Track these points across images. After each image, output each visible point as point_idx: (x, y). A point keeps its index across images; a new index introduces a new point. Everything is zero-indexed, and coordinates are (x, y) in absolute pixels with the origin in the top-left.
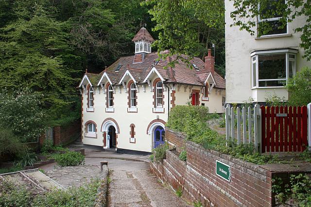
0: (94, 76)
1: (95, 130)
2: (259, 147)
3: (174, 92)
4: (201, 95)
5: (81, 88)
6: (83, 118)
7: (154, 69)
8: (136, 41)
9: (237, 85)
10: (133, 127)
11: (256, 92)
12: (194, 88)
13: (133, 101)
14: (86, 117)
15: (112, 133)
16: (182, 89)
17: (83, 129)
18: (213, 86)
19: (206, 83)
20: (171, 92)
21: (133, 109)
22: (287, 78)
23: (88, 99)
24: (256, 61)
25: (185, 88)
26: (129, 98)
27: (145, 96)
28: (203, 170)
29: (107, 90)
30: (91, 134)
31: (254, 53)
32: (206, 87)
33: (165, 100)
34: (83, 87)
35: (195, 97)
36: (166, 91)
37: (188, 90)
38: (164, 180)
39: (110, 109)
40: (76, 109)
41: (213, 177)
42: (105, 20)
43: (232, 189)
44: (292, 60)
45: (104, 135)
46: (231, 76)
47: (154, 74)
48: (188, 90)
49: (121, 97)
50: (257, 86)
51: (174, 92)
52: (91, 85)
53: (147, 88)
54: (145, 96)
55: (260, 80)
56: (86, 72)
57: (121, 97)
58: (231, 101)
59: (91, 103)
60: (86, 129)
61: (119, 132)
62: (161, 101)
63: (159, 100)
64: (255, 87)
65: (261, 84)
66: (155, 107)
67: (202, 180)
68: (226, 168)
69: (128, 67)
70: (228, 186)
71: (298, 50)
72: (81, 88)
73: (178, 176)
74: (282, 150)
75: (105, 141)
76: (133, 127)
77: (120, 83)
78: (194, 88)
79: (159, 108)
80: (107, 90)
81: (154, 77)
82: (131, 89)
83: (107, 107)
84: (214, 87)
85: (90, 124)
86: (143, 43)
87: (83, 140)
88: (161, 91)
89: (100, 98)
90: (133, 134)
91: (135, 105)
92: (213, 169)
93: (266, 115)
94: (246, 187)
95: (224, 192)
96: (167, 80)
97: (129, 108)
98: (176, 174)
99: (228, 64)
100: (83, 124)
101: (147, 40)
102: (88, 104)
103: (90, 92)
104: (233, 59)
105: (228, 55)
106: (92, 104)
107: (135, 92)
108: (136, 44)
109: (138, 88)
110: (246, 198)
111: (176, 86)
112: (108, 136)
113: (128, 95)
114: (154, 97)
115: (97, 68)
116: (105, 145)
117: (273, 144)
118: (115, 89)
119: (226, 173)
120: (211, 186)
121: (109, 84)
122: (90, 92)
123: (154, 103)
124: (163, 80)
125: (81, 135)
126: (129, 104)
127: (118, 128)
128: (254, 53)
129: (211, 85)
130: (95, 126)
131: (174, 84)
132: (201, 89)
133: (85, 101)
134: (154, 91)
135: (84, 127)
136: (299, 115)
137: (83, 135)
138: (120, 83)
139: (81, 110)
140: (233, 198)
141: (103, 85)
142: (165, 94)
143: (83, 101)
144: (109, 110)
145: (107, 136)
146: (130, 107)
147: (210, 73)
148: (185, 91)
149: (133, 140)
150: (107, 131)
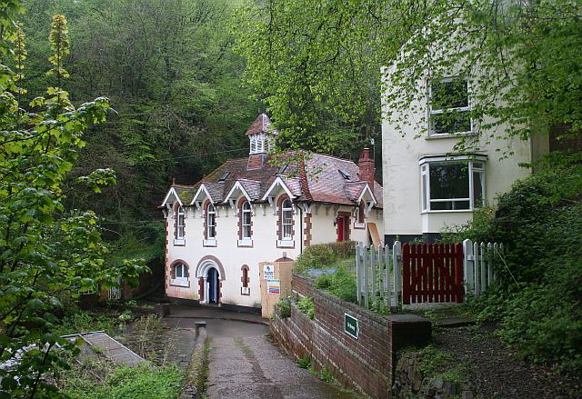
0: (186, 189)
1: (187, 275)
2: (400, 297)
3: (309, 215)
4: (353, 220)
5: (165, 207)
6: (167, 256)
7: (278, 180)
8: (251, 135)
9: (399, 207)
10: (245, 270)
11: (426, 216)
12: (340, 209)
13: (246, 229)
14: (173, 253)
15: (213, 277)
16: (322, 210)
17: (168, 273)
18: (371, 205)
19: (359, 200)
20: (305, 216)
21: (246, 241)
22: (471, 199)
23: (176, 226)
24: (427, 172)
25: (317, 208)
26: (240, 224)
27: (265, 222)
28: (331, 328)
29: (206, 213)
30: (181, 281)
31: (424, 161)
32: (361, 207)
33: (296, 228)
34: (168, 207)
35: (343, 225)
36: (297, 214)
37: (331, 211)
38: (287, 347)
39: (211, 241)
40: (156, 240)
41: (342, 336)
42: (202, 98)
43: (360, 348)
44: (477, 170)
45: (201, 283)
46: (392, 193)
47: (279, 188)
48: (331, 211)
49: (228, 223)
50: (428, 210)
51: (309, 215)
52: (181, 204)
53: (196, 212)
54: (265, 222)
55: (433, 200)
56: (174, 185)
57: (228, 223)
58: (391, 231)
59: (180, 231)
60: (173, 272)
61: (224, 278)
62: (289, 230)
63: (285, 228)
64: (425, 211)
65: (434, 206)
66: (280, 239)
67: (331, 341)
68: (353, 323)
69: (242, 173)
70: (355, 344)
71: (486, 156)
72: (165, 207)
73: (305, 338)
74: (431, 301)
75: (202, 292)
76: (245, 270)
77: (226, 201)
78: (340, 209)
79: (286, 241)
80: (206, 213)
81: (278, 192)
82: (244, 211)
83: (206, 238)
84: (374, 208)
85: (179, 266)
86: (262, 138)
87: (167, 291)
88: (289, 214)
89: (195, 223)
90: (246, 281)
91: (249, 236)
92: (342, 324)
93: (456, 255)
94: (372, 343)
95: (351, 352)
96: (298, 197)
97: (279, 242)
98: (303, 336)
99: (387, 175)
100: (168, 265)
101: (269, 134)
102: (176, 234)
103: (179, 214)
104: (395, 168)
105: (386, 162)
106: (183, 234)
107: (249, 215)
108: (252, 139)
109: (255, 209)
110: (372, 357)
111: (312, 206)
112: (207, 285)
113: (277, 218)
114: (279, 223)
115: (190, 176)
116: (202, 299)
117: (419, 293)
118: (255, 209)
119: (353, 328)
120: (340, 347)
121: (244, 199)
122: (179, 214)
123: (279, 233)
124: (292, 197)
125: (164, 282)
126: (240, 233)
127: (223, 271)
128: (424, 161)
129: (369, 204)
130: (186, 268)
131: (309, 203)
132: (353, 211)
133: (171, 229)
134: (279, 213)
135: (170, 269)
136: (453, 255)
137: (167, 282)
138: (226, 201)
139: (165, 242)
140: (361, 359)
141: (200, 204)
142: (296, 218)
143: (168, 229)
144: (209, 243)
145: (205, 282)
146: (241, 238)
147: (367, 186)
148: (327, 214)
149: (245, 291)
150: (205, 276)
